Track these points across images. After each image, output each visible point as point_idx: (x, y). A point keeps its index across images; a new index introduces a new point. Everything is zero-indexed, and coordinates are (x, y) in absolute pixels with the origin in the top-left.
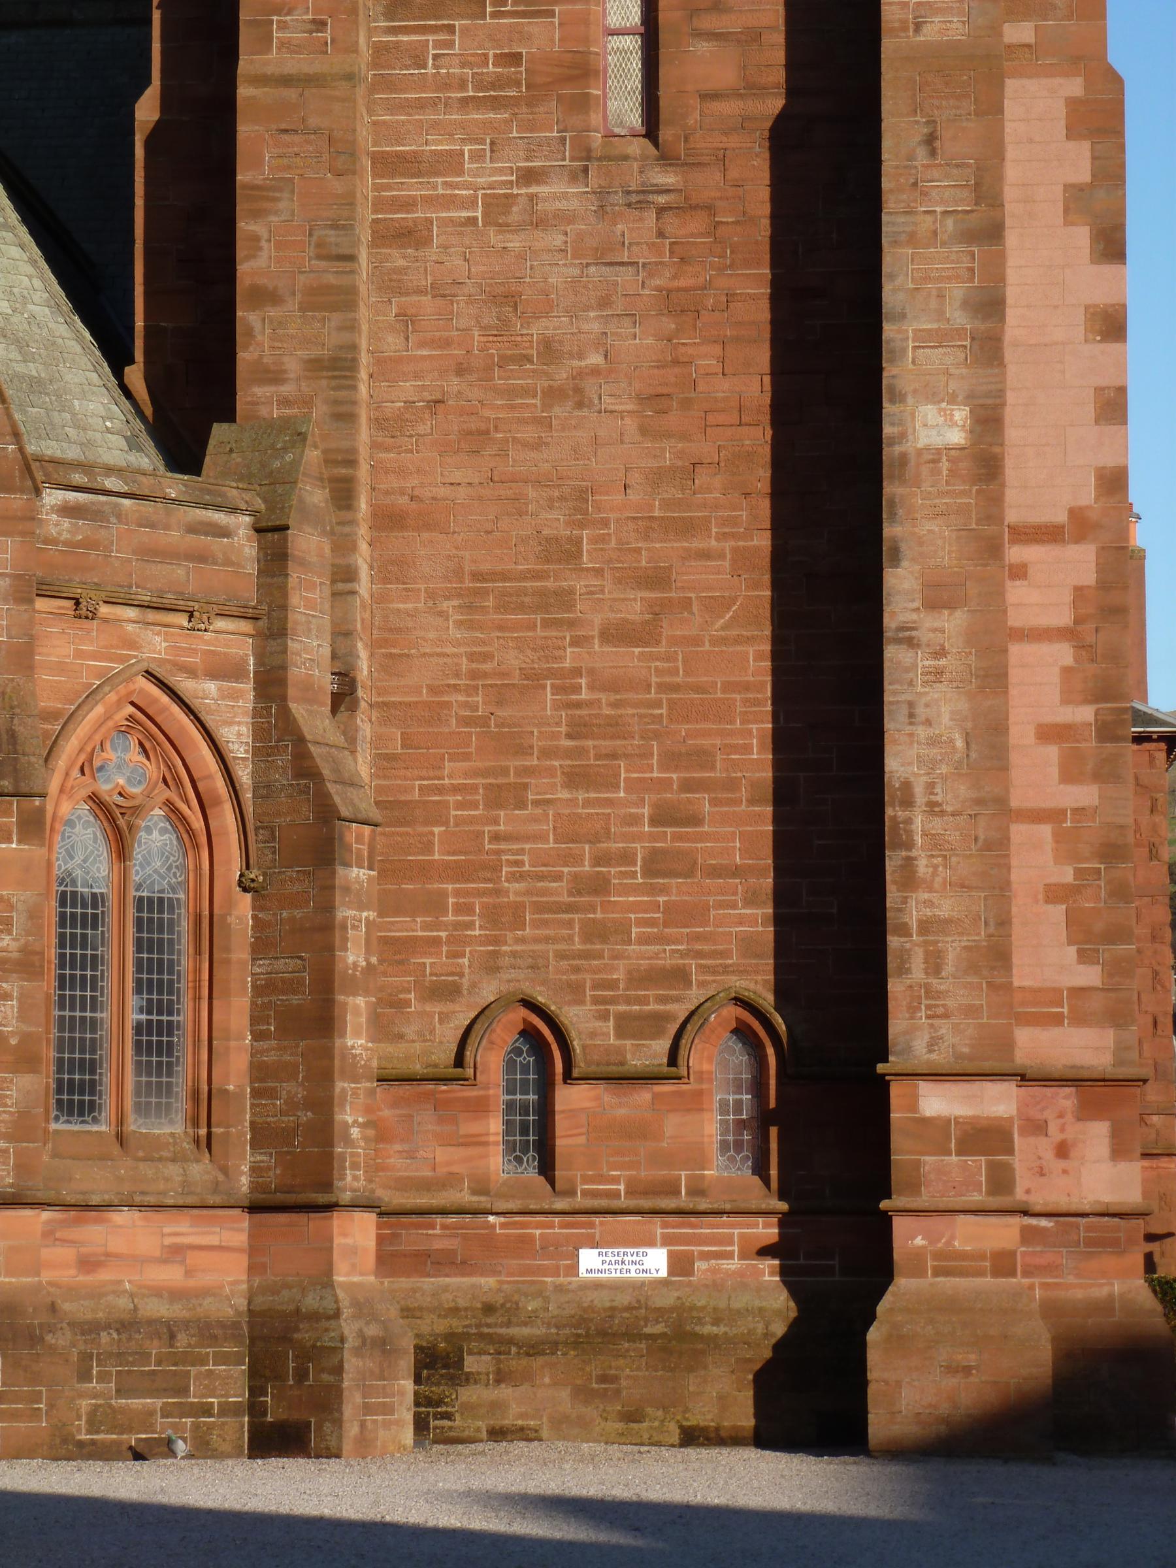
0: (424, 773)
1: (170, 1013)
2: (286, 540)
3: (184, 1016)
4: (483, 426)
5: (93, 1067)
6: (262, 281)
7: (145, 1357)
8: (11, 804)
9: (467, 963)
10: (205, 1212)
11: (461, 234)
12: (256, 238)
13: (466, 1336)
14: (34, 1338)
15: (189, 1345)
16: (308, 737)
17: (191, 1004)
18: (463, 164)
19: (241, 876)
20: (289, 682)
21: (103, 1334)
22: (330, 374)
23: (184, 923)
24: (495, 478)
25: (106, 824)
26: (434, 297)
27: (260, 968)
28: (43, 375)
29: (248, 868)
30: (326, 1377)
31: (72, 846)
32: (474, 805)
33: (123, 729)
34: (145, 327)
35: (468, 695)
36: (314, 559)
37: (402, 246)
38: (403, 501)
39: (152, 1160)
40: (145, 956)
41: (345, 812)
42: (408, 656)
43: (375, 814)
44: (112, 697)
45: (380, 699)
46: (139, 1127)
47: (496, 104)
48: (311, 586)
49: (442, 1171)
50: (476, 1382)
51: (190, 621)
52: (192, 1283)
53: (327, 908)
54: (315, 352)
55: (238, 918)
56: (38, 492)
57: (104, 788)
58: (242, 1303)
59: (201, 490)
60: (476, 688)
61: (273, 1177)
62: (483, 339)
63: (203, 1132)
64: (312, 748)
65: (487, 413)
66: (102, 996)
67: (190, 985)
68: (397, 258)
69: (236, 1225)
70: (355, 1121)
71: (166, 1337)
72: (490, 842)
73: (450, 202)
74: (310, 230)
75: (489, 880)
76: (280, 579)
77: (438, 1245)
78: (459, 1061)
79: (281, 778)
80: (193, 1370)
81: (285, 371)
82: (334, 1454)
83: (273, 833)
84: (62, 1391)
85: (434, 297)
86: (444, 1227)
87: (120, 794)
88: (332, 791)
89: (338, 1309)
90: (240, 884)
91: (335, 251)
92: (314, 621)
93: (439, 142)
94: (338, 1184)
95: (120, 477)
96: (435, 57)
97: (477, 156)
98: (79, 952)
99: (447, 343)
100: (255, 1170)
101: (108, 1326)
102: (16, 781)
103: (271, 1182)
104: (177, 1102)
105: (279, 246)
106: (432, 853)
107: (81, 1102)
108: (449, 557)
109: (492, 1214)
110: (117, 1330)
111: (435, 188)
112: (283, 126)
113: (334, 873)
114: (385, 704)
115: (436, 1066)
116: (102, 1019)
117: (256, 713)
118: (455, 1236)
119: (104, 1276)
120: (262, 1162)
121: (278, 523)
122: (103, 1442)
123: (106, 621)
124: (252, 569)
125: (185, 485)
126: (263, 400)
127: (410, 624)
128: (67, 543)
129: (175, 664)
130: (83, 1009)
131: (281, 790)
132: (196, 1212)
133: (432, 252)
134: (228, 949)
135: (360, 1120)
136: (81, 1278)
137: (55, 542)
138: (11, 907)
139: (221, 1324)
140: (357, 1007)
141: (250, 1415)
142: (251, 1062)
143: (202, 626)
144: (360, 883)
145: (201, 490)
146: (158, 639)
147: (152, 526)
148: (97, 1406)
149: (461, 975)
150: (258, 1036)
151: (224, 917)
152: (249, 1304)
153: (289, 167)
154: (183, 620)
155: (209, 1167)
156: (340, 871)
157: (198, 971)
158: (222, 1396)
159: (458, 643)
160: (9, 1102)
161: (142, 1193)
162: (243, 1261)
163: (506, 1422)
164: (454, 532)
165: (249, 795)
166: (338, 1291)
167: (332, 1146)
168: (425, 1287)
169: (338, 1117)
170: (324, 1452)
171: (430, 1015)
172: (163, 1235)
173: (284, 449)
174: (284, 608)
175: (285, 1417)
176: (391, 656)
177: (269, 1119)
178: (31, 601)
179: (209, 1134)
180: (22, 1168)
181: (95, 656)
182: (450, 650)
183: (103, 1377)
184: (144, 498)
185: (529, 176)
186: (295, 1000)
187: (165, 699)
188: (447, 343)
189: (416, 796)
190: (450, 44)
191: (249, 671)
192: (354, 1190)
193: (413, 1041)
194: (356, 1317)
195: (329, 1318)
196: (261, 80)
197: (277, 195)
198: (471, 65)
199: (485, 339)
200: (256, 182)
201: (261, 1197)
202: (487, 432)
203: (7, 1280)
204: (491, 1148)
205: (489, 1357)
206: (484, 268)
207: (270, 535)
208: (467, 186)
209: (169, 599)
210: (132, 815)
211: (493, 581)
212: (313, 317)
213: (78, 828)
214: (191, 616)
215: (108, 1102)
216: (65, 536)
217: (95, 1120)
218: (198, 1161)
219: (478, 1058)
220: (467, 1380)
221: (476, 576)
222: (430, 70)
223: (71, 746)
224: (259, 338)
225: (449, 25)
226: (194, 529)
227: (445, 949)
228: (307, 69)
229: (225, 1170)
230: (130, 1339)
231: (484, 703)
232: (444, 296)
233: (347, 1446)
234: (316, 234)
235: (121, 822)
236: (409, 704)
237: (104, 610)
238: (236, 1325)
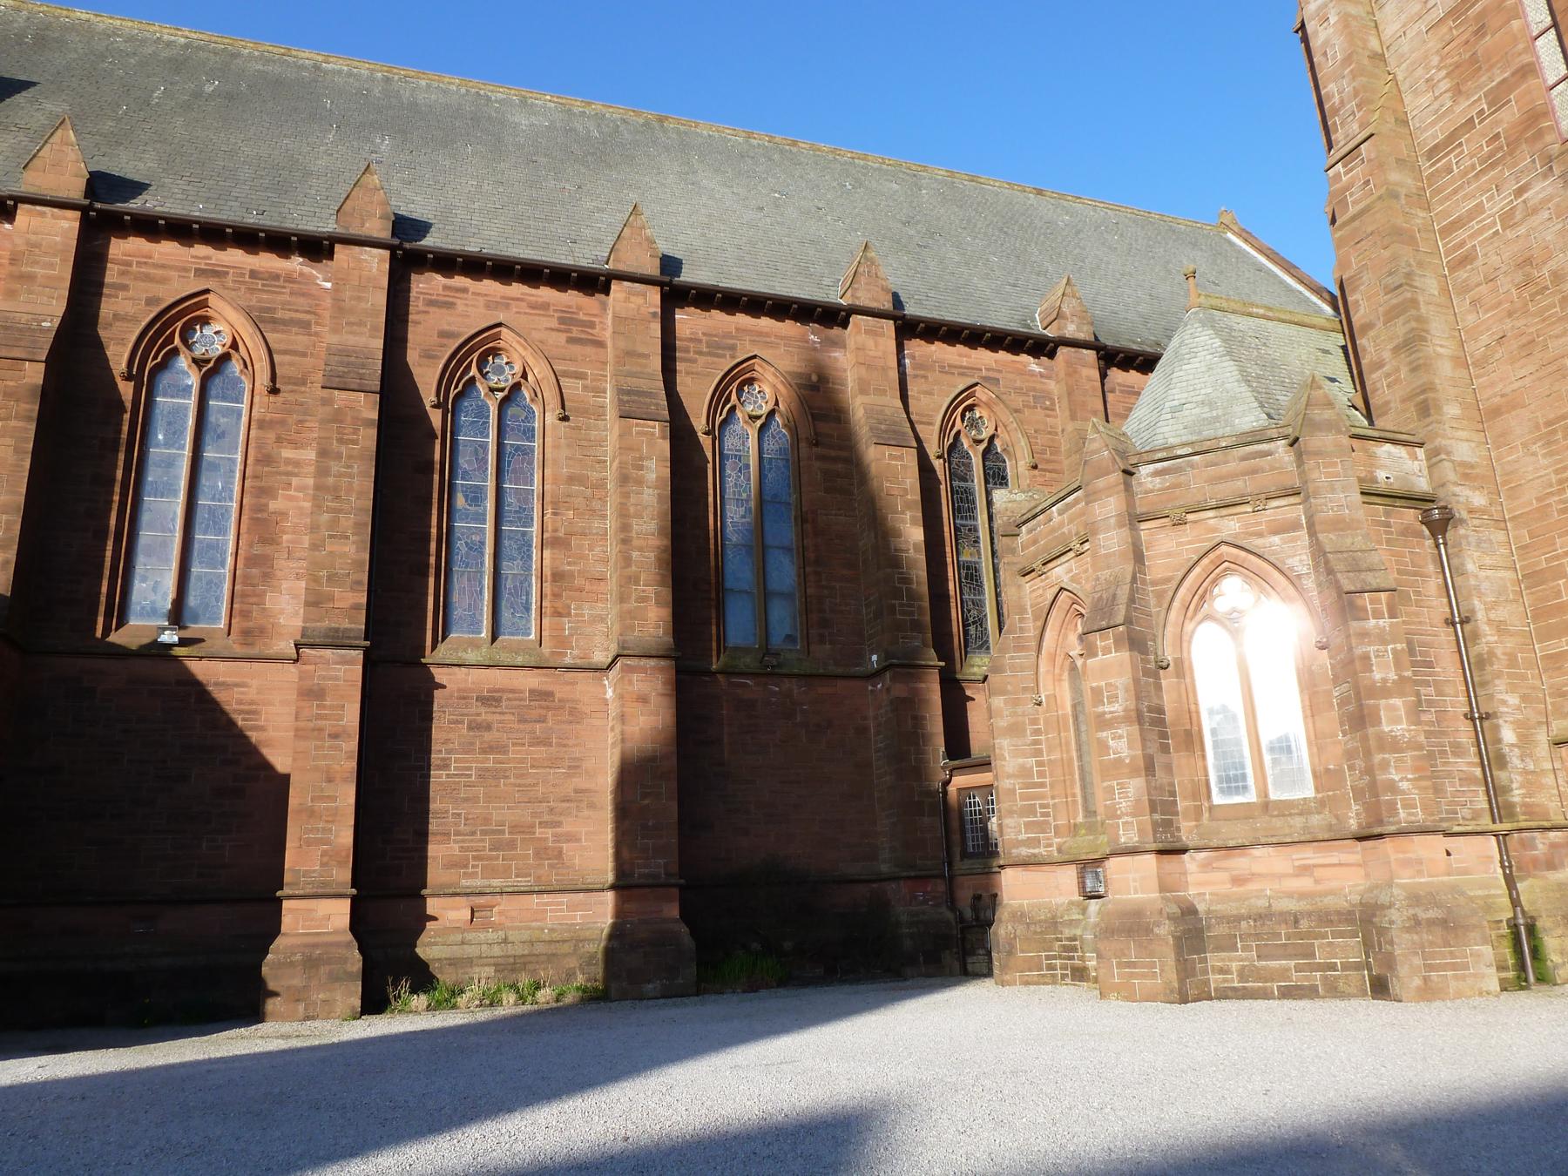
4: (1530, 338)
6: (1363, 321)
12: (1357, 301)
38: (1497, 400)
39: (1284, 815)
47: (1493, 166)
52: (1319, 888)
54: (1396, 342)
68: (1462, 274)
80: (1316, 942)
91: (1392, 287)
97: (1490, 199)
106: (1561, 597)
108: (1529, 420)
119: (1252, 886)
122: (1252, 988)
123: (1195, 522)
128: (1158, 490)
133: (1479, 262)
136: (1235, 889)
137: (1152, 491)
139: (1339, 913)
140: (1393, 708)
146: (1232, 523)
147: (1216, 465)
148: (1243, 967)
172: (1293, 860)
181: (1190, 543)
183: (1246, 948)
185: (1520, 192)
187: (1243, 554)
188: (1500, 304)
189: (1544, 565)
198: (1475, 155)
216: (1158, 486)
221: (1548, 424)
226: (1244, 459)
237: (1190, 517)
238: (1350, 913)
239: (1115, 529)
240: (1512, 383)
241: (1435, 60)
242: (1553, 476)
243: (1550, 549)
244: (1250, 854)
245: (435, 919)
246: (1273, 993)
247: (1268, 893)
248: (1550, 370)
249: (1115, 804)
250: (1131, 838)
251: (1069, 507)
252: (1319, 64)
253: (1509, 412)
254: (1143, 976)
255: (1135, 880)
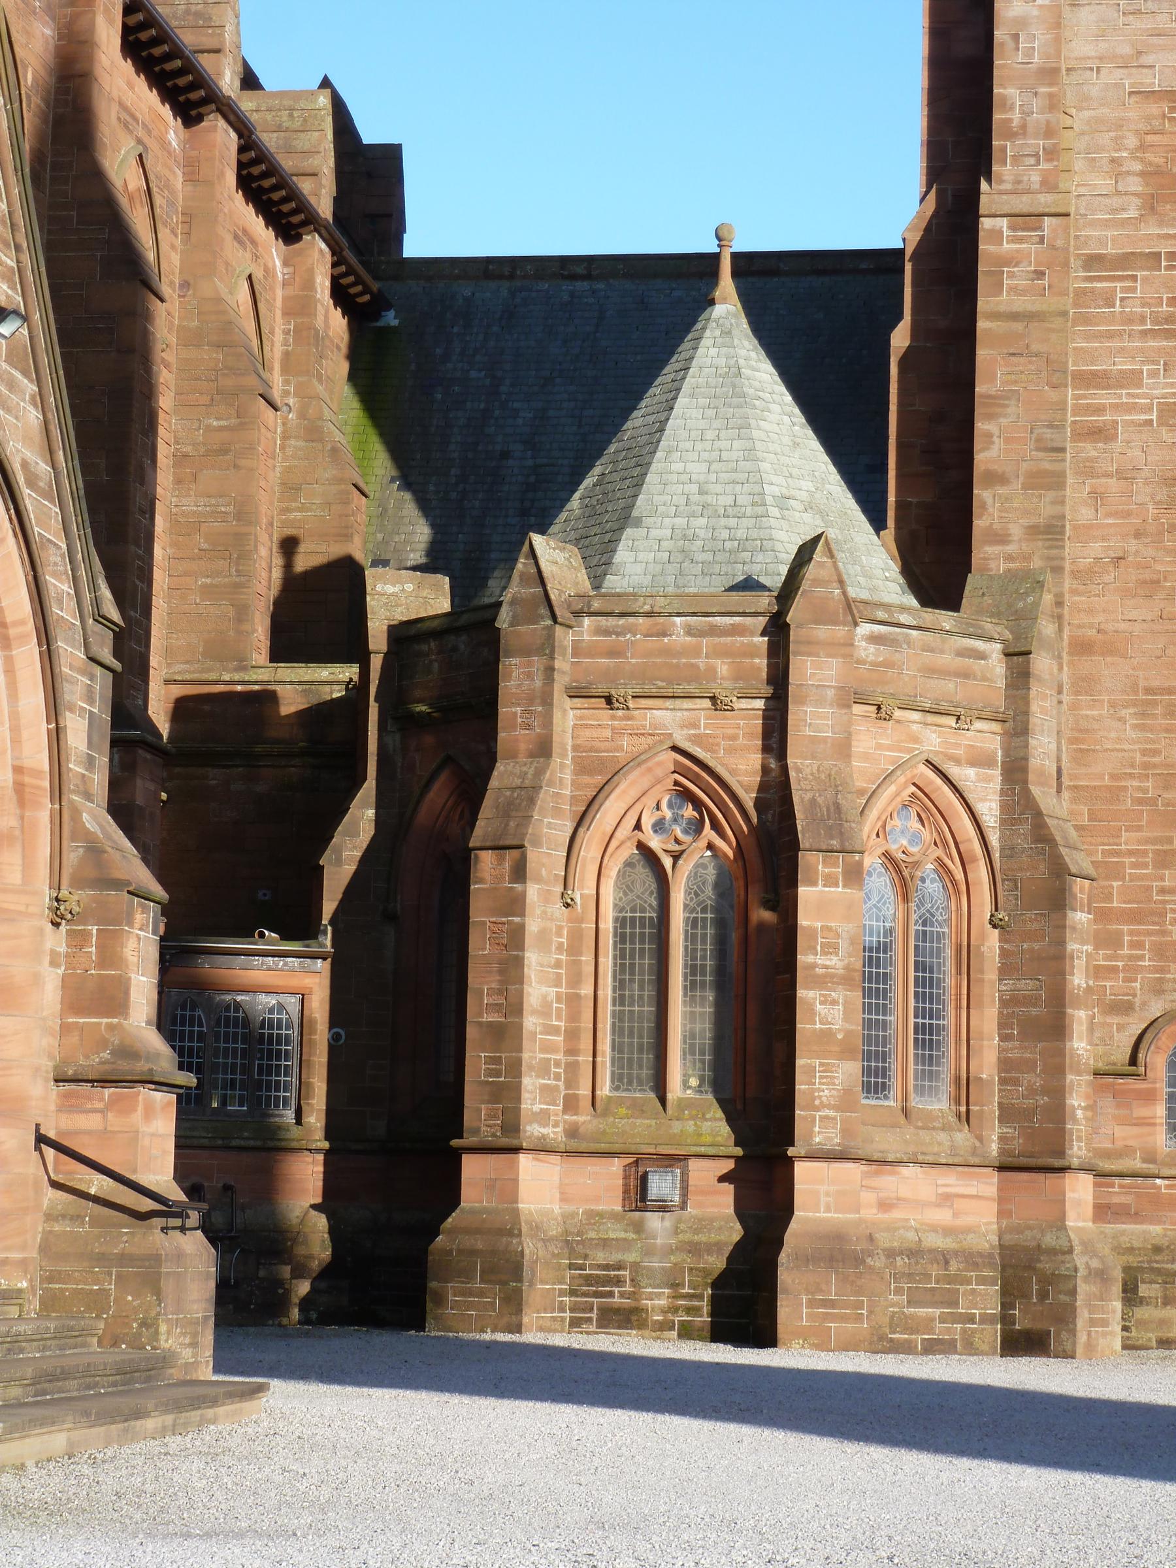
0: (1106, 840)
1: (938, 1019)
2: (1028, 662)
3: (949, 1020)
4: (1155, 577)
5: (884, 1057)
7: (927, 1277)
8: (838, 858)
9: (1139, 987)
10: (966, 1169)
11: (1140, 432)
12: (989, 435)
13: (1140, 1269)
14: (857, 1260)
15: (959, 1270)
16: (1045, 812)
17: (953, 1012)
18: (1142, 380)
19: (992, 916)
20: (1030, 770)
21: (898, 1259)
22: (1044, 537)
23: (948, 951)
24: (1164, 617)
25: (894, 874)
26: (1118, 479)
27: (1008, 985)
28: (839, 537)
29: (996, 910)
30: (1063, 1298)
31: (870, 891)
32: (1145, 865)
33: (906, 803)
34: (896, 501)
35: (1140, 782)
36: (1047, 677)
37: (1095, 441)
38: (1092, 633)
39: (928, 1129)
40: (920, 974)
41: (1074, 870)
42: (1094, 750)
43: (1091, 871)
44: (902, 779)
45: (1072, 784)
46: (916, 1103)
48: (1044, 697)
49: (1119, 1144)
50: (1148, 1304)
51: (957, 722)
52: (959, 1222)
53: (1061, 943)
54: (1034, 521)
55: (988, 948)
56: (856, 624)
57: (893, 847)
58: (994, 1239)
59: (967, 624)
60: (1147, 776)
61: (1017, 1145)
62: (1155, 511)
63: (963, 1109)
64: (1048, 820)
65: (1159, 567)
66: (890, 1004)
67: (953, 997)
68: (1090, 450)
69: (988, 1181)
70: (1080, 1105)
71: (942, 1262)
72: (1157, 894)
73: (1132, 408)
74: (1031, 429)
75: (1154, 924)
76: (1024, 691)
77: (1116, 1200)
78: (1133, 1061)
79: (1023, 842)
80: (962, 1288)
81: (1010, 535)
82: (1070, 1355)
83: (1016, 885)
84: (879, 1301)
85: (1118, 479)
86: (1121, 1186)
87: (903, 852)
88: (1064, 853)
89: (1071, 1247)
90: (991, 921)
92: (1046, 723)
93: (1125, 363)
94: (1068, 1152)
95: (910, 614)
96: (1122, 299)
97: (1154, 374)
98: (874, 970)
99: (1128, 514)
100: (1002, 1139)
101: (901, 1253)
102: (842, 843)
103: (1015, 1149)
104: (943, 1085)
105: (1008, 441)
107: (876, 1083)
108: (1127, 676)
109: (1159, 1178)
110: (908, 1256)
111: (1120, 397)
112: (1011, 351)
113: (1065, 915)
114: (1076, 787)
115: (1115, 1064)
116: (890, 1021)
117: (1003, 792)
118: (1131, 1193)
119: (896, 1214)
120: (1008, 1133)
121: (1023, 649)
122: (898, 1340)
123: (898, 722)
124: (1001, 683)
125: (955, 620)
126: (992, 556)
127: (1096, 726)
128: (873, 664)
129: (946, 755)
130: (877, 1014)
131: (1023, 852)
132: (960, 1169)
133: (1117, 446)
134: (982, 971)
135: (1083, 1104)
136: (880, 1216)
137: (864, 662)
138: (838, 936)
139: (981, 1255)
140: (1080, 1018)
141: (1003, 1323)
142: (999, 1058)
143: (966, 727)
144: (1083, 924)
145: (967, 624)
146: (934, 736)
147: (932, 650)
149: (1134, 995)
150: (1004, 1038)
151: (978, 947)
152: (1000, 1240)
153: (1016, 382)
154: (951, 721)
155: (969, 1135)
156: (1070, 914)
157: (959, 986)
158: (982, 1309)
159: (1134, 742)
160: (837, 1082)
161: (923, 1153)
162: (994, 1207)
163: (1171, 1335)
164: (1131, 657)
165: (998, 855)
166: (1070, 1233)
167: (1065, 1123)
168: (1107, 1231)
169: (1068, 1102)
170: (1061, 1354)
171: (1110, 1025)
173: (1027, 594)
174: (1026, 713)
175: (1029, 1326)
176: (1081, 750)
177: (1013, 1101)
178: (850, 707)
179: (968, 1111)
180: (846, 1132)
181: (890, 748)
182: (1127, 746)
184: (927, 629)
186: (1034, 1011)
187: (939, 781)
188: (1128, 514)
190: (1134, 289)
191: (997, 760)
192: (1079, 1158)
193: (1097, 1045)
194: (1084, 1253)
195: (1064, 1253)
196: (995, 316)
197: (1006, 402)
198: (1149, 305)
199: (1158, 511)
200: (990, 393)
201: (1009, 1161)
202: (1158, 582)
203: (836, 1215)
204: (1158, 1128)
205: (1158, 1286)
206: (1157, 458)
207: (1015, 658)
208: (1145, 396)
209: (944, 706)
210: (913, 867)
211: (1162, 694)
212: (1032, 495)
213: (874, 876)
214: (958, 718)
215: (896, 1084)
216: (871, 658)
217: (886, 1097)
218: (960, 1131)
219: (1148, 1060)
220: (1141, 1303)
221: (1148, 691)
222: (1118, 309)
223: (873, 814)
224: (991, 510)
225: (1133, 275)
226: (962, 653)
227: (1121, 975)
228: (1030, 307)
229: (980, 1138)
230: (917, 1263)
231: (1154, 788)
232: (1126, 479)
233: (1080, 1350)
234: (1036, 432)
235: (906, 873)
236: (1095, 787)
237: (898, 714)
238: (991, 1255)
239: (831, 705)
240: (1118, 622)
241: (1132, 141)
242: (1138, 755)
243: (1111, 840)
244: (898, 1173)
245: (722, 1179)
246: (916, 1346)
247: (913, 1223)
248: (1169, 627)
249: (814, 1091)
250: (830, 1139)
251: (713, 631)
252: (1002, 44)
253: (1103, 654)
254: (844, 1318)
255: (827, 1194)
